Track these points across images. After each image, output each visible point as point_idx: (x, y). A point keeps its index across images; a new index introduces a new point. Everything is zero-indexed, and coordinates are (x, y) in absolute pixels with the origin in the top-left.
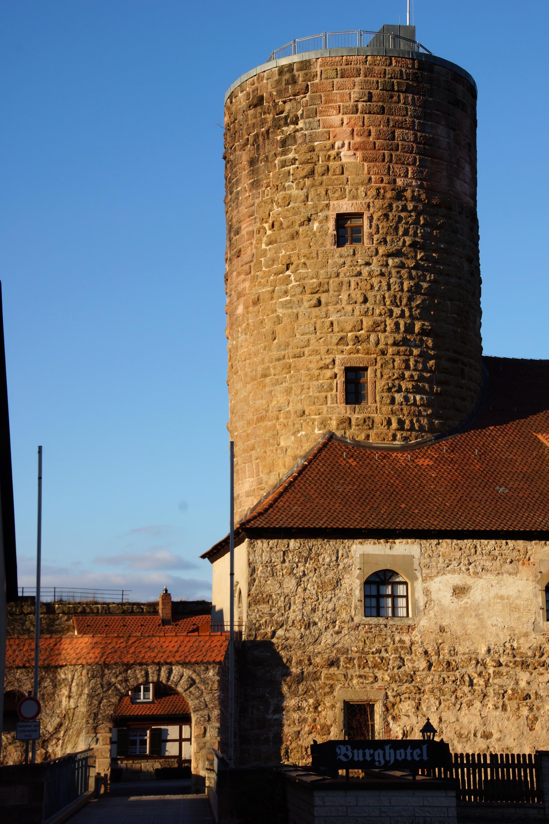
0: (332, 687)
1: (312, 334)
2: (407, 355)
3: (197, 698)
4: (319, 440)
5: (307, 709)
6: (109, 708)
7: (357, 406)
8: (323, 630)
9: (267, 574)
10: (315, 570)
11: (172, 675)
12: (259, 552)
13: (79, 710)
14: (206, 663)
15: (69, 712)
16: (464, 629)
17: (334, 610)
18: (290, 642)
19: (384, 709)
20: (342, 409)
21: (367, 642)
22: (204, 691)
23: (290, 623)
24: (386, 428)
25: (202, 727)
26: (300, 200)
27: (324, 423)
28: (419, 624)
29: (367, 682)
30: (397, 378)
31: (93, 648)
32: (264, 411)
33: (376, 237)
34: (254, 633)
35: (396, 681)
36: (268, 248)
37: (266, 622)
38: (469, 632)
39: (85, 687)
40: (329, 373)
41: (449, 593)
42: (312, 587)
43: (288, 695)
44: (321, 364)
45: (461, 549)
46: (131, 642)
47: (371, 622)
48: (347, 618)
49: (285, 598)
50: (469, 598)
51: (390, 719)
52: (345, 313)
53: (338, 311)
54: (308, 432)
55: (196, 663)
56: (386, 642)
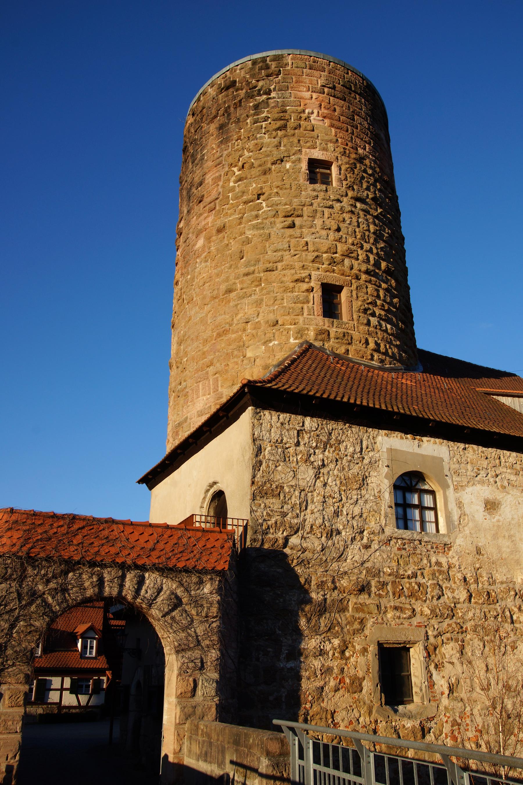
0: (362, 622)
1: (285, 251)
2: (377, 286)
3: (184, 629)
4: (296, 349)
5: (331, 653)
7: (335, 320)
8: (349, 542)
10: (337, 461)
11: (144, 588)
12: (266, 426)
14: (199, 572)
16: (499, 552)
18: (308, 555)
19: (425, 654)
20: (324, 323)
21: (401, 562)
23: (308, 528)
24: (364, 346)
25: (191, 679)
26: (273, 145)
27: (300, 333)
28: (455, 543)
29: (405, 616)
31: (9, 529)
33: (345, 183)
34: (261, 537)
35: (437, 616)
36: (236, 185)
37: (276, 523)
38: (504, 555)
41: (481, 508)
42: (334, 483)
43: (306, 632)
44: (296, 277)
45: (487, 458)
46: (76, 527)
47: (404, 536)
48: (377, 529)
49: (300, 493)
50: (500, 515)
51: (432, 667)
52: (318, 234)
53: (313, 233)
54: (282, 341)
56: (422, 564)
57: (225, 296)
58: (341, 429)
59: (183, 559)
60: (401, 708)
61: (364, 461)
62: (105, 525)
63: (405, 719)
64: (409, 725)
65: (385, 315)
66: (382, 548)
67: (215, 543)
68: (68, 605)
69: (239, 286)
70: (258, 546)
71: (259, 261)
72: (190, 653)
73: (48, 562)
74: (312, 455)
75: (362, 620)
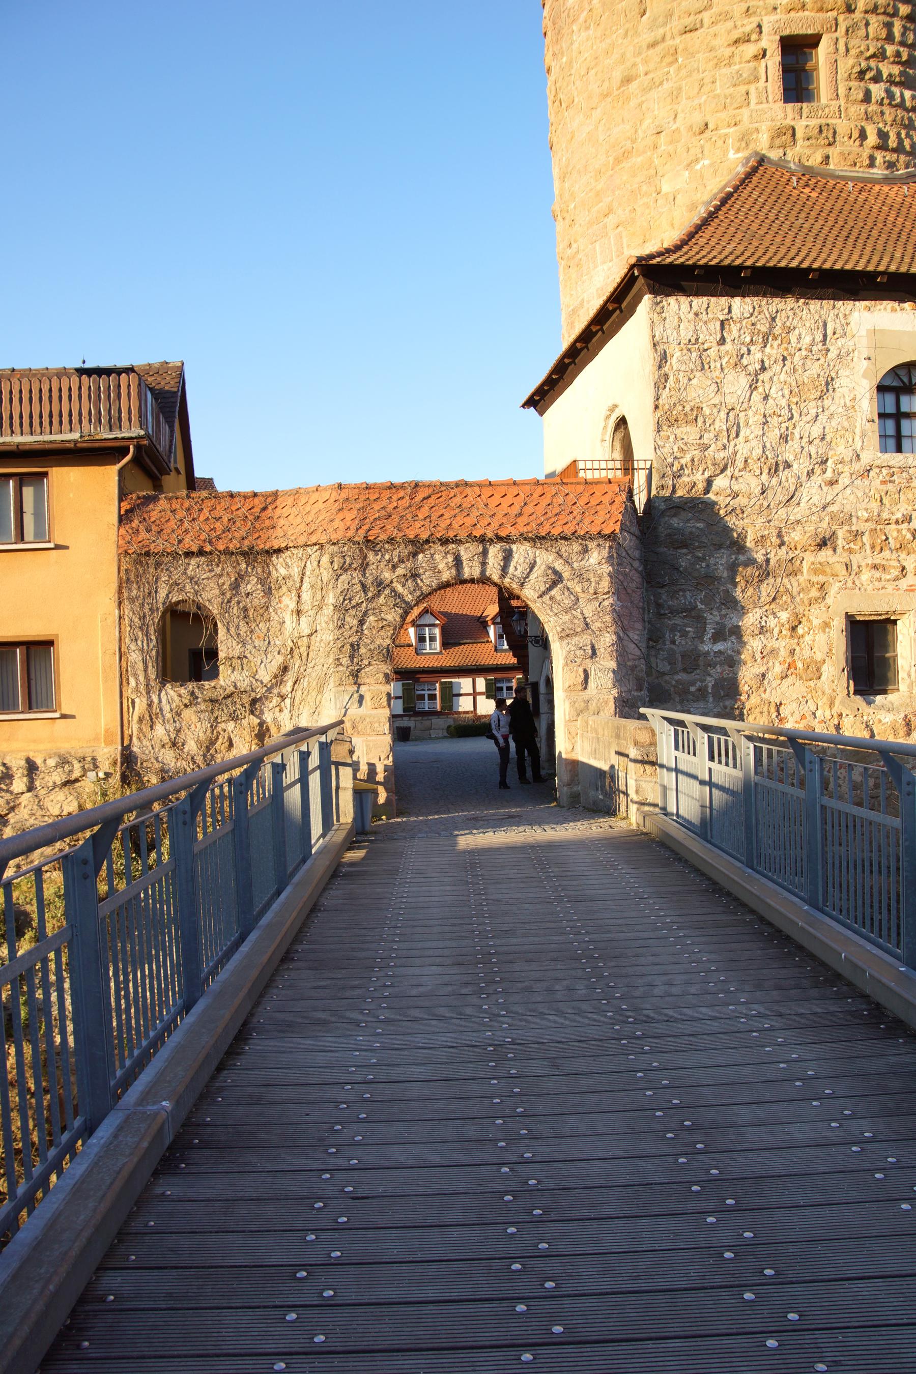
2: (888, 15)
6: (382, 633)
7: (805, 105)
9: (691, 366)
10: (784, 359)
11: (513, 564)
12: (671, 322)
13: (318, 639)
14: (583, 538)
15: (300, 644)
17: (823, 439)
18: (741, 501)
20: (784, 113)
21: (885, 501)
22: (581, 595)
23: (740, 464)
24: (857, 143)
25: (581, 670)
27: (745, 139)
29: (888, 577)
30: (873, 56)
32: (629, 142)
34: (671, 483)
37: (693, 460)
39: (327, 590)
40: (751, 50)
42: (780, 393)
44: (736, 35)
46: (420, 497)
48: (848, 454)
49: (728, 414)
55: (562, 538)
57: (622, 89)
58: (792, 309)
59: (559, 523)
60: (879, 699)
61: (829, 354)
62: (456, 490)
63: (882, 712)
64: (887, 720)
65: (901, 74)
66: (856, 482)
67: (603, 498)
68: (422, 593)
69: (641, 69)
70: (667, 495)
71: (671, 16)
72: (577, 639)
73: (392, 544)
74: (745, 356)
75: (822, 586)
